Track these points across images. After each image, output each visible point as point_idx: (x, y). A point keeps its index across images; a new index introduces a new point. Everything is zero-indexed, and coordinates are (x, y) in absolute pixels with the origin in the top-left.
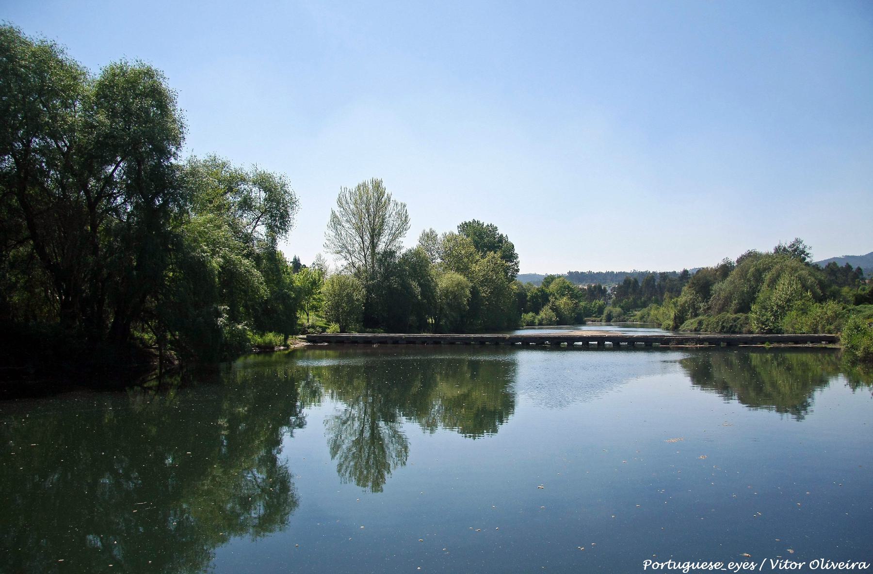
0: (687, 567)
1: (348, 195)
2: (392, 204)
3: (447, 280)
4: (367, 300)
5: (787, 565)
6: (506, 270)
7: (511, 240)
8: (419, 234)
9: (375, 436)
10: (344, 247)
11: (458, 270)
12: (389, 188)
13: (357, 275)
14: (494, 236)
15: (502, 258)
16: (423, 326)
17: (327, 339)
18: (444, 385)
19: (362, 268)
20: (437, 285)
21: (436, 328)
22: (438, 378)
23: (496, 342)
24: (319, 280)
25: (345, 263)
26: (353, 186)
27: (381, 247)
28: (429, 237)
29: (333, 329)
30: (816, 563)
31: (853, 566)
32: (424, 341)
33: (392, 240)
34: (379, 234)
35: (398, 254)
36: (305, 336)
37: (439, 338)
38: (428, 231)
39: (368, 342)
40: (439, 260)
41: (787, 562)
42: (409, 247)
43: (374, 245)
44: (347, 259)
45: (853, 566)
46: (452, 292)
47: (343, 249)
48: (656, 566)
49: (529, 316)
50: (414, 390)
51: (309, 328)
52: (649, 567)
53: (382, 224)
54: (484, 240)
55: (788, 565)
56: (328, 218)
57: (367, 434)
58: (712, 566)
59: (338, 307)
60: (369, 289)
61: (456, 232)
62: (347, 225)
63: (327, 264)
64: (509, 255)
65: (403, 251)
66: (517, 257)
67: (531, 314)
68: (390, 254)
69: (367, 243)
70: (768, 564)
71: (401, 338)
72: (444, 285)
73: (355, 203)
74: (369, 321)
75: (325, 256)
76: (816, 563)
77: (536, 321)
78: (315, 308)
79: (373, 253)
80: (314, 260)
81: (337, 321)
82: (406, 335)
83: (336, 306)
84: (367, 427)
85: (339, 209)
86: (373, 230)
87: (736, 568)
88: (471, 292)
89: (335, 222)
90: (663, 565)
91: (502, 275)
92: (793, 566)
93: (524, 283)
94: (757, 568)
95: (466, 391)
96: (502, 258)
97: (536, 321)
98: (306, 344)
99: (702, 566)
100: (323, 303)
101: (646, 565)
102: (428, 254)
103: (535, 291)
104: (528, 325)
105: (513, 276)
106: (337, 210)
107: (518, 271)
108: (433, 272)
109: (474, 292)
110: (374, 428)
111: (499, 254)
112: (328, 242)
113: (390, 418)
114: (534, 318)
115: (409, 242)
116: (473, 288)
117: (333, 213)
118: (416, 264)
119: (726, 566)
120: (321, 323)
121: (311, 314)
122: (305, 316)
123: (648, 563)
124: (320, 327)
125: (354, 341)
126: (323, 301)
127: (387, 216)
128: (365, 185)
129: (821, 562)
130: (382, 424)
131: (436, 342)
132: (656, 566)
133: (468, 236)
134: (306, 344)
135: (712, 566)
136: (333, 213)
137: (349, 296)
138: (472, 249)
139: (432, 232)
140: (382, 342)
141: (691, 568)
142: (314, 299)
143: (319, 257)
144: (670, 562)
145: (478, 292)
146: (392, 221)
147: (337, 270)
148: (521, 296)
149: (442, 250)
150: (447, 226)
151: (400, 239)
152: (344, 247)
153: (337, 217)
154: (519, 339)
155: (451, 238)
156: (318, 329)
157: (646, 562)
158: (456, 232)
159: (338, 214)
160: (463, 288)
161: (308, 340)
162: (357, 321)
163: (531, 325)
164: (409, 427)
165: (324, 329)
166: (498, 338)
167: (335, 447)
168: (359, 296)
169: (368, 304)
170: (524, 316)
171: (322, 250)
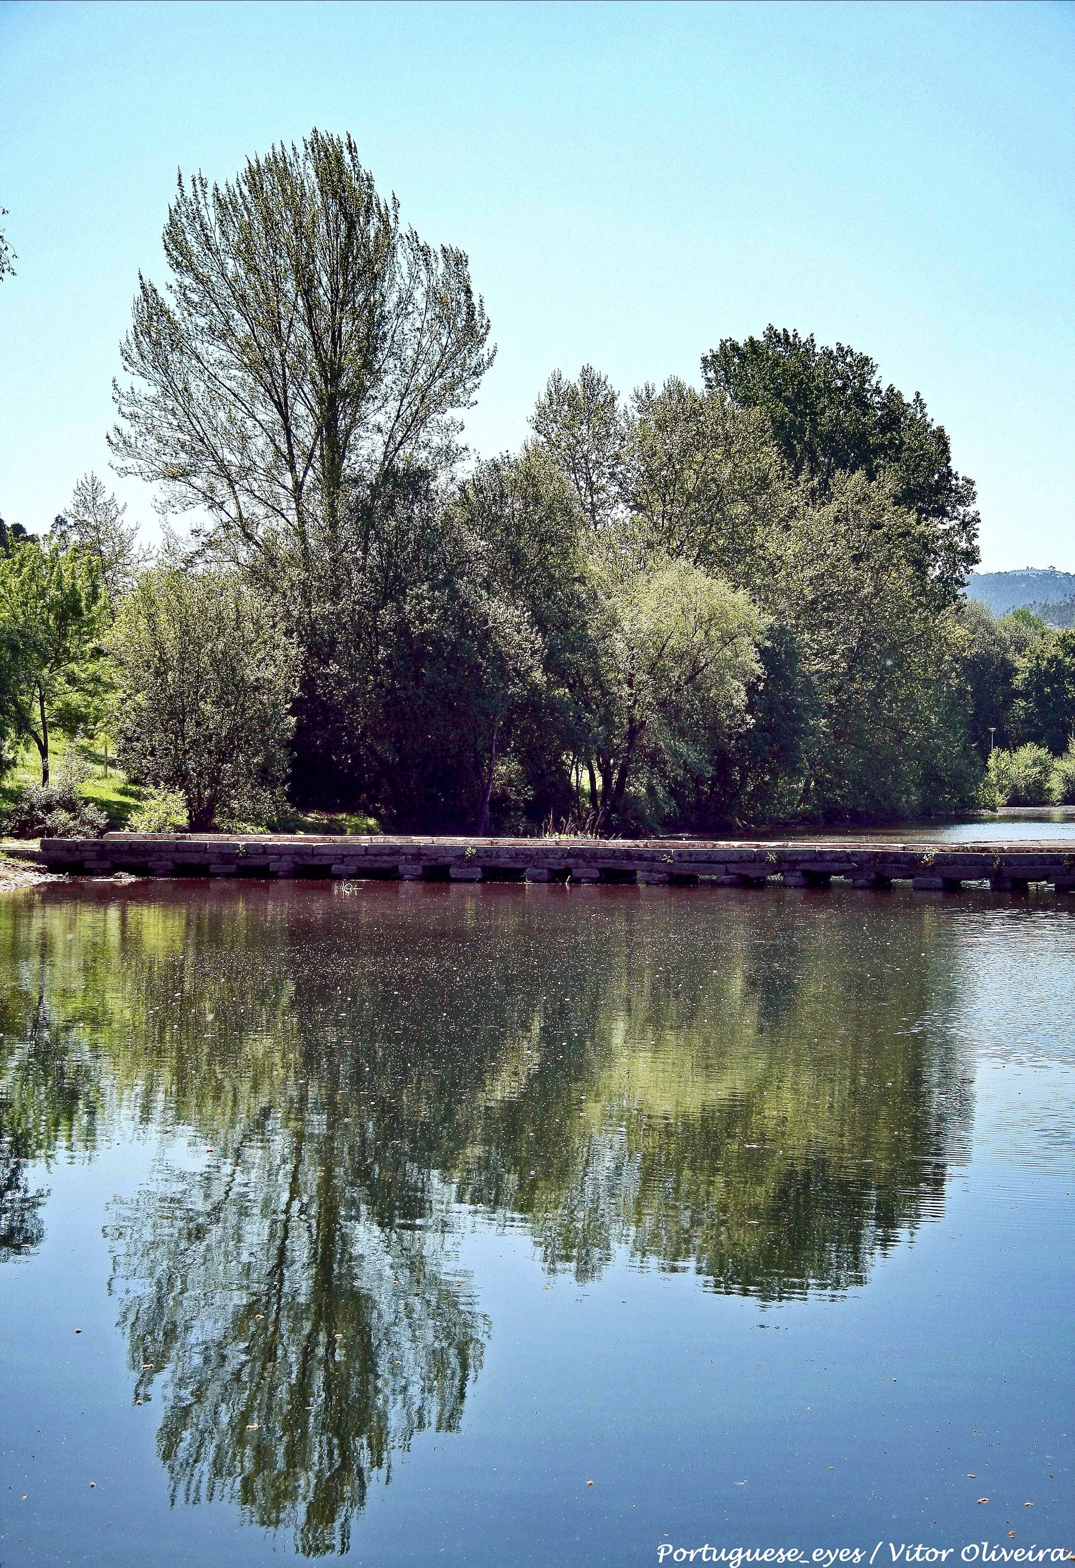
0: (739, 1556)
1: (210, 215)
2: (402, 258)
3: (662, 606)
4: (307, 684)
5: (919, 1554)
6: (920, 554)
7: (937, 416)
8: (538, 390)
9: (337, 1297)
10: (201, 448)
11: (705, 557)
12: (388, 171)
13: (262, 576)
14: (860, 400)
15: (906, 498)
16: (552, 803)
17: (140, 858)
18: (643, 1062)
19: (285, 547)
20: (614, 622)
21: (615, 812)
22: (618, 1031)
23: (878, 877)
24: (94, 596)
25: (207, 520)
26: (227, 173)
27: (367, 450)
28: (578, 405)
29: (159, 814)
30: (973, 1550)
31: (1041, 1555)
32: (559, 871)
33: (418, 421)
34: (358, 395)
35: (441, 482)
36: (34, 845)
37: (628, 854)
38: (572, 377)
39: (312, 871)
40: (621, 513)
41: (920, 1548)
42: (490, 453)
43: (334, 443)
44: (217, 506)
45: (1041, 1555)
46: (679, 657)
47: (194, 461)
48: (680, 1555)
49: (1020, 762)
50: (503, 1088)
51: (48, 808)
52: (668, 1559)
53: (369, 348)
54: (819, 421)
55: (922, 1554)
56: (124, 322)
57: (301, 1281)
58: (784, 1556)
59: (178, 715)
60: (319, 648)
61: (696, 382)
62: (214, 352)
63: (125, 522)
64: (932, 485)
65: (465, 470)
66: (966, 496)
67: (1028, 753)
68: (410, 482)
69: (306, 433)
70: (885, 1552)
71: (460, 855)
72: (646, 624)
73: (246, 252)
74: (319, 770)
75: (114, 487)
76: (973, 1550)
77: (1056, 785)
78: (71, 721)
79: (333, 478)
80: (64, 503)
81: (178, 779)
82: (482, 841)
83: (172, 712)
84: (301, 1248)
85: (172, 277)
86: (332, 372)
87: (828, 1559)
88: (766, 656)
89: (156, 334)
90: (692, 1555)
91: (899, 580)
92: (932, 1555)
93: (999, 613)
94: (865, 1559)
95: (741, 1087)
96: (906, 498)
97: (1056, 785)
98: (37, 879)
99: (765, 1556)
100: (112, 699)
101: (662, 1555)
102: (572, 485)
103: (1052, 651)
104: (1015, 801)
105: (950, 584)
106: (164, 277)
107: (971, 557)
108: (595, 567)
109: (779, 657)
110: (330, 1252)
111: (890, 482)
112: (125, 426)
113: (401, 1208)
114: (1046, 771)
115: (492, 428)
116: (776, 634)
117: (148, 292)
118: (526, 527)
119: (808, 1556)
120: (106, 786)
121: (57, 742)
122: (33, 758)
123: (667, 1550)
124: (103, 805)
125: (252, 870)
126: (110, 687)
127: (389, 306)
128: (278, 167)
129: (981, 1548)
130: (365, 1236)
131: (615, 876)
132: (680, 1555)
133: (746, 401)
134: (37, 879)
135: (784, 1556)
136: (148, 292)
137: (227, 665)
138: (770, 457)
139: (591, 382)
140: (380, 872)
141: (744, 1560)
142: (72, 680)
143: (89, 493)
144: (706, 1548)
145: (794, 656)
146: (412, 330)
147: (170, 550)
148: (988, 674)
149: (633, 468)
150: (657, 350)
151: (453, 414)
152: (201, 448)
153: (163, 312)
154: (979, 861)
155: (672, 409)
156: (89, 812)
157: (662, 1548)
158: (696, 382)
159: (170, 301)
160: (728, 639)
161: (48, 860)
162: (264, 777)
163: (1029, 799)
164: (482, 1248)
165: (117, 816)
166: (884, 858)
167: (155, 1337)
168: (274, 666)
169: (312, 707)
170: (997, 760)
171: (100, 461)
